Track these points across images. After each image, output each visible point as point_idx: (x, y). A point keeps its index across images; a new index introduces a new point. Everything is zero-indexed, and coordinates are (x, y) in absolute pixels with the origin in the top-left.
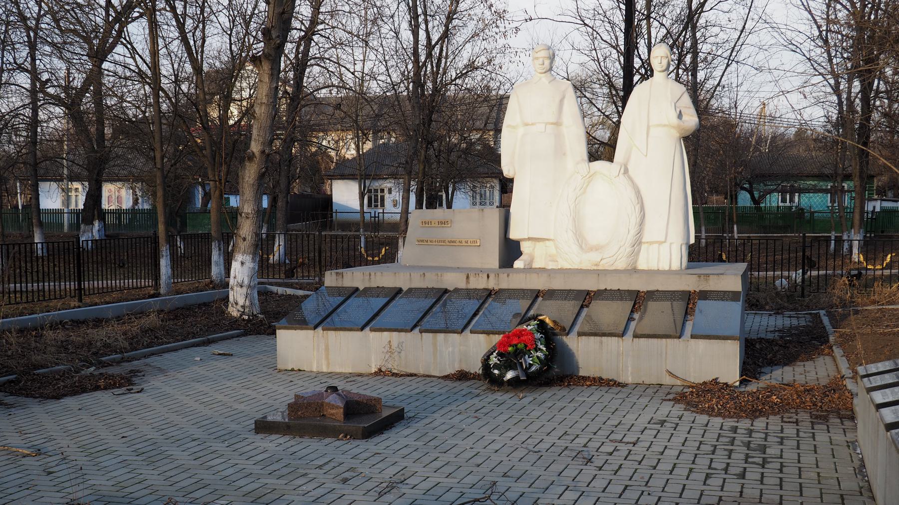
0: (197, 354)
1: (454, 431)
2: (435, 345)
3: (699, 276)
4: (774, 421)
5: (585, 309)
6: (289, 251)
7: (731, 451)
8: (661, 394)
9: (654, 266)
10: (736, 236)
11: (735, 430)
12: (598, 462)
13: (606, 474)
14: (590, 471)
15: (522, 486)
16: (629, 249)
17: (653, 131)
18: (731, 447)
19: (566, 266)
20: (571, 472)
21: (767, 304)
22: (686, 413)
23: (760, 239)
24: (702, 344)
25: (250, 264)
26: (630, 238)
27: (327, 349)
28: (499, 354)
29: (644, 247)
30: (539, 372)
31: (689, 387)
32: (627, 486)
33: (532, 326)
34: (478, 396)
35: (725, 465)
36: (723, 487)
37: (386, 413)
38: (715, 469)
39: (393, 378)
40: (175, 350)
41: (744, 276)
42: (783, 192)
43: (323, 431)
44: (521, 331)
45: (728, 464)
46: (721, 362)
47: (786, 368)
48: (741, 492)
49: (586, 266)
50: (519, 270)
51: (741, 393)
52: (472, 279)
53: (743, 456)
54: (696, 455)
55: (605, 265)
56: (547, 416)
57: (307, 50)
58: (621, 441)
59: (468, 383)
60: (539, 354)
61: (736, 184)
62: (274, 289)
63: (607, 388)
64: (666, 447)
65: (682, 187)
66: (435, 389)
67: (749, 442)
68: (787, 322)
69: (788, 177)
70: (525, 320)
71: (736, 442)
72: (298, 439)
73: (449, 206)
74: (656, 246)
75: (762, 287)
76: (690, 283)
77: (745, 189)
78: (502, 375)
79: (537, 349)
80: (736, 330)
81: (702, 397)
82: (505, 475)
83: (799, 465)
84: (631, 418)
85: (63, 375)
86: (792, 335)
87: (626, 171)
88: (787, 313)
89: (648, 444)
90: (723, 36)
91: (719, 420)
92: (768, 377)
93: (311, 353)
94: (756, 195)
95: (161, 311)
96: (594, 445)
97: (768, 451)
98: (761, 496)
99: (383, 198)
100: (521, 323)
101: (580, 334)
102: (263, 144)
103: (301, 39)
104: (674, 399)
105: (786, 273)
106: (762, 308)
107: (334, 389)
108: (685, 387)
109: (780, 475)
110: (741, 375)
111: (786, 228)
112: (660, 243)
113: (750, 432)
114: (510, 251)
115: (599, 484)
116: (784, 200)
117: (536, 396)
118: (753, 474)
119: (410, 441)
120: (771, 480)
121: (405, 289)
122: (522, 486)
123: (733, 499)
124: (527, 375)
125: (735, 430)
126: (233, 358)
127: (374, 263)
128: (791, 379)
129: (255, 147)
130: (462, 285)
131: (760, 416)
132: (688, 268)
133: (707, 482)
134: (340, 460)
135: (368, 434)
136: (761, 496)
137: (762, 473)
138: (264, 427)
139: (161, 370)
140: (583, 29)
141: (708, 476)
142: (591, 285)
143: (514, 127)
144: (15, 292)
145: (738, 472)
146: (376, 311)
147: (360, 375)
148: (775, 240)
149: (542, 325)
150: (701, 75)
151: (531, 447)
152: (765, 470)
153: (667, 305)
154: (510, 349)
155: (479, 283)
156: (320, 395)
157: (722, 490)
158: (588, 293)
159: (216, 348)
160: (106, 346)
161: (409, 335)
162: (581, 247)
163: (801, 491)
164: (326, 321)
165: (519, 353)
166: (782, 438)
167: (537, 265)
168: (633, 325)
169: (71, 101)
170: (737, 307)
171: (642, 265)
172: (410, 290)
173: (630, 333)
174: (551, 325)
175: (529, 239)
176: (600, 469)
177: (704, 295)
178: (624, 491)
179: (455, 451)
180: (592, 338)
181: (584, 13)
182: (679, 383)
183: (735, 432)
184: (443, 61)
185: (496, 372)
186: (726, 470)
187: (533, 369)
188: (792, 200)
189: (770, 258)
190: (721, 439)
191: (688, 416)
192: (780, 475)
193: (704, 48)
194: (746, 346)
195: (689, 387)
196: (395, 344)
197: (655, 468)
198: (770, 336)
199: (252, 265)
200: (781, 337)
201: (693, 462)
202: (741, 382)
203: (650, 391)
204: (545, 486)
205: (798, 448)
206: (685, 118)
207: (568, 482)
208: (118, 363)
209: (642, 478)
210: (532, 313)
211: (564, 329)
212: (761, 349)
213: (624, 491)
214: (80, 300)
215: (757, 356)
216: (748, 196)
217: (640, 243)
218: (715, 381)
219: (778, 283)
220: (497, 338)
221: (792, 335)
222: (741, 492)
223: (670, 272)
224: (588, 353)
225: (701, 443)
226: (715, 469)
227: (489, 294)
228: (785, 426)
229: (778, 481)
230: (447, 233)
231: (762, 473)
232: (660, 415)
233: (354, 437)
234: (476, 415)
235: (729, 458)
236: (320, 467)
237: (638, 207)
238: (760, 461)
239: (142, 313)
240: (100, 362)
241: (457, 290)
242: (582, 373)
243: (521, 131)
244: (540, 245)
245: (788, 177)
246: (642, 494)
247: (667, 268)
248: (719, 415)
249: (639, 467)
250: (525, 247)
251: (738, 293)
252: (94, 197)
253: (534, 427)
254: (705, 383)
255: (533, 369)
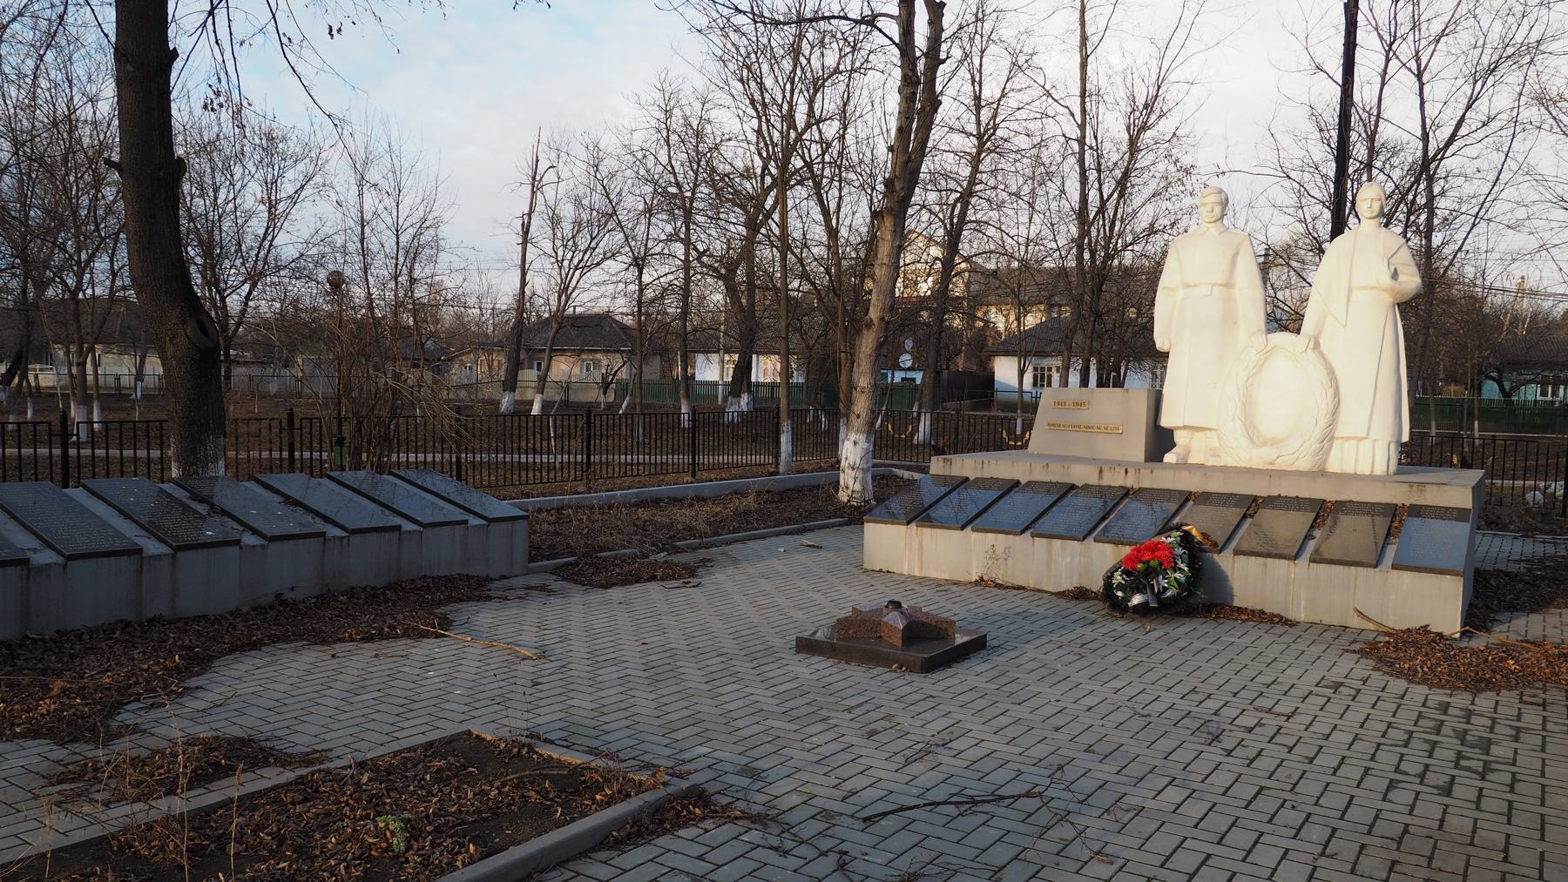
0: (782, 544)
1: (1043, 672)
2: (1049, 553)
3: (1411, 484)
4: (1509, 697)
5: (1249, 520)
6: (935, 431)
7: (1434, 744)
8: (1343, 641)
9: (1349, 468)
10: (1476, 434)
11: (1444, 708)
12: (1228, 743)
13: (1235, 764)
14: (1213, 754)
15: (1106, 771)
16: (1316, 446)
17: (1356, 295)
18: (1434, 738)
19: (1231, 463)
20: (1184, 755)
21: (1512, 522)
22: (1375, 674)
23: (1511, 438)
24: (1407, 578)
25: (863, 445)
26: (1318, 432)
27: (921, 547)
28: (1124, 572)
29: (1337, 444)
30: (1175, 600)
31: (1386, 634)
32: (1262, 788)
33: (1172, 539)
34: (1092, 623)
35: (1420, 768)
36: (1413, 807)
37: (960, 639)
38: (1405, 773)
39: (996, 591)
40: (763, 537)
41: (1477, 489)
42: (1544, 384)
43: (873, 658)
44: (1156, 545)
45: (1427, 766)
46: (1435, 603)
47: (1534, 617)
48: (1442, 821)
49: (1256, 464)
50: (1170, 466)
51: (1461, 650)
52: (1105, 473)
53: (1451, 755)
54: (1379, 745)
55: (1282, 464)
56: (1182, 659)
57: (963, 213)
58: (1270, 711)
59: (1087, 604)
60: (1178, 575)
61: (1480, 373)
62: (899, 472)
63: (1268, 626)
64: (1335, 727)
65: (1393, 367)
66: (1041, 610)
67: (1466, 731)
68: (1540, 549)
69: (1550, 365)
70: (1166, 529)
71: (1445, 730)
72: (843, 665)
73: (1121, 385)
74: (1354, 443)
75: (1507, 500)
76: (1397, 495)
77: (1493, 379)
78: (1127, 599)
79: (1175, 569)
80: (1459, 559)
81: (1399, 651)
82: (1089, 749)
83: (1544, 781)
84: (1293, 672)
85: (624, 560)
86: (1545, 568)
87: (1317, 346)
88: (1540, 537)
89: (1308, 720)
90: (1469, 189)
91: (1422, 690)
92: (1504, 627)
93: (912, 556)
94: (1507, 386)
95: (759, 493)
96: (1230, 712)
97: (1495, 750)
98: (1474, 832)
99: (1050, 377)
100: (1160, 533)
101: (1237, 552)
102: (883, 309)
103: (957, 200)
104: (1361, 651)
105: (1542, 484)
106: (1505, 528)
107: (896, 605)
108: (1380, 633)
109: (1509, 796)
110: (1464, 624)
111: (1544, 428)
112: (1360, 439)
113: (1468, 715)
114: (1161, 441)
115: (1221, 779)
116: (1544, 394)
117: (1168, 628)
118: (1465, 790)
119: (979, 682)
120: (1493, 804)
121: (1023, 482)
122: (1106, 771)
123: (1426, 832)
124: (1159, 601)
125: (1444, 708)
126: (823, 553)
127: (1015, 447)
128: (1540, 633)
129: (874, 314)
130: (1093, 480)
131: (1487, 688)
132: (1398, 473)
133: (1390, 796)
134: (880, 702)
135: (931, 666)
136: (1474, 832)
137: (1481, 790)
138: (806, 646)
139: (735, 561)
140: (1287, 183)
141: (1392, 785)
142: (1260, 489)
143: (1172, 290)
144: (601, 463)
145: (1441, 783)
146: (982, 508)
147: (957, 583)
148: (1534, 440)
149: (1187, 538)
150: (1437, 239)
151: (1139, 708)
152: (1486, 785)
153: (1364, 521)
154: (1140, 566)
155: (1115, 479)
156: (878, 612)
157: (1411, 813)
158: (1255, 499)
159: (806, 539)
160: (690, 528)
161: (1018, 539)
162: (1251, 440)
163: (1543, 823)
164: (921, 515)
165: (1150, 573)
166: (1518, 730)
167: (1192, 460)
168: (1311, 545)
169: (726, 270)
170: (1464, 528)
171: (1334, 465)
172: (1029, 483)
173: (1307, 554)
174: (1199, 538)
175: (1185, 427)
176: (1229, 753)
177: (1417, 511)
178: (1255, 797)
179: (1035, 702)
180: (1253, 559)
181: (1287, 164)
182: (1371, 626)
183: (1445, 713)
184: (1118, 223)
185: (1120, 594)
186: (1422, 777)
187: (1169, 593)
188: (1554, 394)
189: (1521, 464)
190: (1422, 722)
191: (1378, 679)
192: (1509, 796)
193: (1443, 205)
194: (1476, 581)
195: (1386, 634)
196: (1000, 549)
197: (1311, 761)
198: (1513, 568)
199: (865, 446)
200: (1529, 570)
201: (1372, 759)
202: (1463, 633)
203: (1329, 635)
204: (1140, 775)
205: (1543, 750)
206: (1401, 278)
207: (1176, 770)
208: (694, 549)
209: (1289, 776)
210: (1177, 520)
211: (1215, 545)
212: (1498, 587)
213: (1255, 797)
214: (694, 476)
215: (1488, 596)
216: (1496, 386)
217: (1332, 438)
218: (1425, 630)
219: (1529, 496)
220: (1126, 550)
221: (1545, 568)
222: (1442, 821)
223: (1371, 478)
224: (1247, 578)
225: (1390, 725)
226: (1405, 773)
227: (1126, 493)
228: (1526, 709)
229: (1504, 807)
230: (1084, 416)
231: (1481, 790)
232: (1335, 676)
233: (911, 669)
234: (1082, 651)
235: (1430, 756)
236: (849, 710)
237: (1330, 392)
238: (1478, 766)
239: (741, 493)
240: (674, 547)
241: (1086, 487)
242: (1237, 603)
243: (1181, 294)
244: (1198, 435)
245: (1550, 365)
246: (1282, 805)
247: (1367, 472)
248: (1424, 681)
249: (1288, 756)
250: (1179, 437)
251: (1466, 511)
252: (743, 369)
253: (1152, 676)
254: (1409, 630)
255: (1169, 593)
